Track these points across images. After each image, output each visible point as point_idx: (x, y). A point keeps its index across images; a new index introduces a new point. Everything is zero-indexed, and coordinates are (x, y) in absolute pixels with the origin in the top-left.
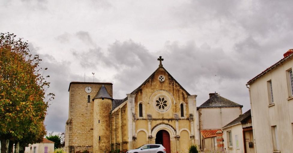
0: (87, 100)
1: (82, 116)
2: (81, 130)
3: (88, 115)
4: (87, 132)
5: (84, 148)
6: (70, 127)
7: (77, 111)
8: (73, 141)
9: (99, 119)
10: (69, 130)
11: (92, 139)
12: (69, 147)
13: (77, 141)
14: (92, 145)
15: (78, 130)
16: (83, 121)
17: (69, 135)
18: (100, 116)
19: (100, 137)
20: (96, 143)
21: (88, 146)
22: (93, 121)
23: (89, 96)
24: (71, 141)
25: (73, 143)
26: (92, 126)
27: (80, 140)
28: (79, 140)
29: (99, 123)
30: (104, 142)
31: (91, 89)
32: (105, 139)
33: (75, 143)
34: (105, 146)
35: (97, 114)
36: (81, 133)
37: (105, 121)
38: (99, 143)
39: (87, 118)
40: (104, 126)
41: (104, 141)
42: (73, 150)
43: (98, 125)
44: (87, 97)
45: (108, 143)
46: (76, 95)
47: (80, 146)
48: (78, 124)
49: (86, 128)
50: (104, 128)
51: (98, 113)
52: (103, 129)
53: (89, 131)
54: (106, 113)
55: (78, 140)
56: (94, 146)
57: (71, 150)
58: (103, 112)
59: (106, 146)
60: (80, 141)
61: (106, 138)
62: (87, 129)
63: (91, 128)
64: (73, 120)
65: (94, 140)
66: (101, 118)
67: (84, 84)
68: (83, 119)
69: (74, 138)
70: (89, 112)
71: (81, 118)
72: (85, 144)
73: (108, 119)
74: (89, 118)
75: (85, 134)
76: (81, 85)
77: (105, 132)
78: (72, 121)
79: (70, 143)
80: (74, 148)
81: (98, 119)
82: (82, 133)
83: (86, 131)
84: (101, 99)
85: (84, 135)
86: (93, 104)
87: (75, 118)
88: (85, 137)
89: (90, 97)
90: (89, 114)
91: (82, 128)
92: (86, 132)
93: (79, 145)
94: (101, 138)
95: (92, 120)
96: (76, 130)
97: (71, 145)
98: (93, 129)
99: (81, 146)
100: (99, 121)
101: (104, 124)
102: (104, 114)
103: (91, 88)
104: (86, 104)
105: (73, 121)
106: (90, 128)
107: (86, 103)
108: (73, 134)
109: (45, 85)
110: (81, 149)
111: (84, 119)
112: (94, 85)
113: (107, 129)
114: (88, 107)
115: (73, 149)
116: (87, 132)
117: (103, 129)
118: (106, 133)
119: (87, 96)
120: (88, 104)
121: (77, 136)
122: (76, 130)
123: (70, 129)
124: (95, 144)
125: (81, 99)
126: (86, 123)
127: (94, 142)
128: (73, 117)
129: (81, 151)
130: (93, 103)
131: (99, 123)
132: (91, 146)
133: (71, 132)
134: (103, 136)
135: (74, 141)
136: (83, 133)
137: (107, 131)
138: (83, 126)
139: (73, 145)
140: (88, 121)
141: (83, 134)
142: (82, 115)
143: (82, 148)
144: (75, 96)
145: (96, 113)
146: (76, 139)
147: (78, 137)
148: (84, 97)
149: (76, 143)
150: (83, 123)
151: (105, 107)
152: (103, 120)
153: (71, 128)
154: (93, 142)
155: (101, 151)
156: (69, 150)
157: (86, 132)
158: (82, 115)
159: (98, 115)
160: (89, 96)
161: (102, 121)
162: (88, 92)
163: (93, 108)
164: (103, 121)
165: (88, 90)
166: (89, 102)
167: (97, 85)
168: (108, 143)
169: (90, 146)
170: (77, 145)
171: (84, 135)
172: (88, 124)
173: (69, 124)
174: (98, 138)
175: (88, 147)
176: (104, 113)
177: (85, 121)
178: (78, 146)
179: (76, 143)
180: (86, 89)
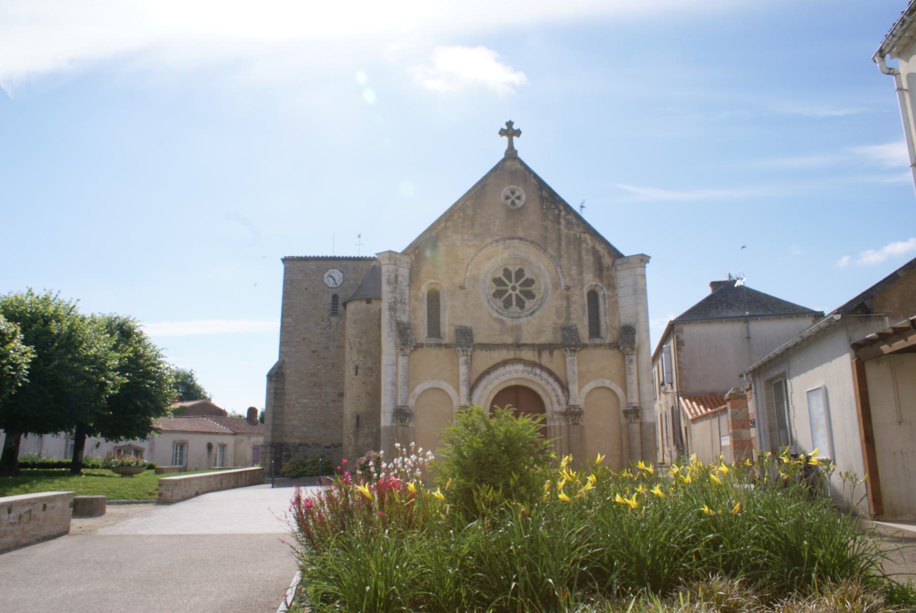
6: (108, 573)
18: (359, 352)
19: (358, 417)
21: (329, 444)
44: (330, 300)
81: (353, 362)
120: (333, 319)
131: (356, 374)
169: (336, 444)
174: (354, 421)
175: (329, 447)
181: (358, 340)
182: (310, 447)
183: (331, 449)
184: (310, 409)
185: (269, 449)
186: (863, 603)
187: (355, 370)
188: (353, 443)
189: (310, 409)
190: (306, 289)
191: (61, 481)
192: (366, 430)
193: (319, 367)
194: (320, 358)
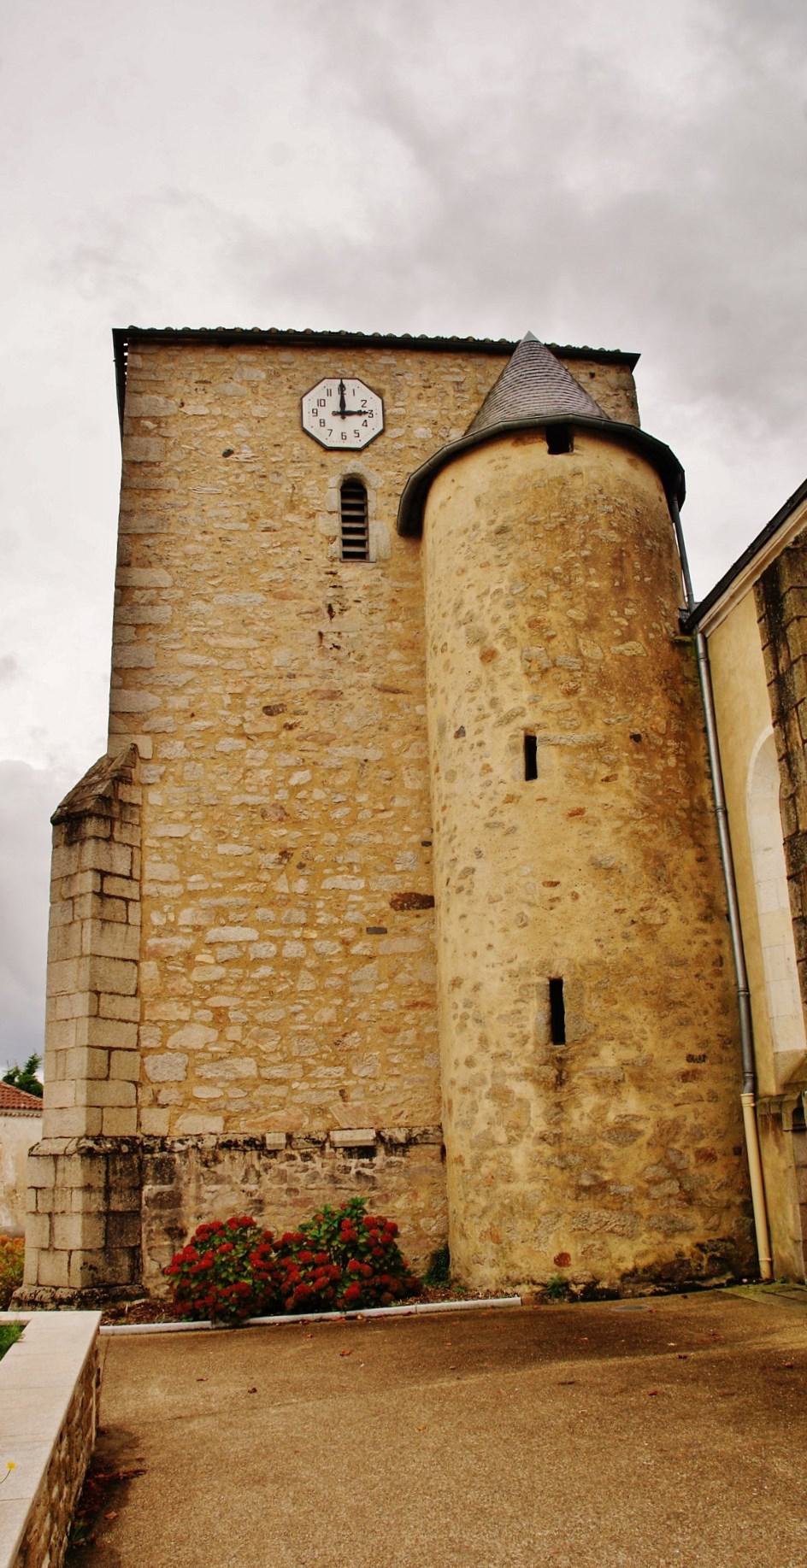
0: (331, 524)
1: (271, 724)
2: (270, 914)
3: (349, 719)
4: (345, 943)
5: (316, 1164)
6: (103, 874)
7: (199, 659)
8: (150, 1061)
9: (529, 720)
10: (87, 906)
11: (429, 1045)
12: (89, 1154)
13: (207, 1071)
14: (422, 1121)
15: (221, 915)
16: (282, 795)
17: (85, 977)
18: (540, 673)
19: (556, 986)
20: (501, 1095)
21: (366, 1137)
22: (425, 797)
23: (354, 490)
24: (124, 1065)
25: (155, 1102)
26: (407, 858)
27: (256, 1053)
28: (237, 1050)
29: (531, 772)
30: (640, 1076)
31: (374, 403)
32: (640, 1017)
33: (188, 1103)
34: (648, 1129)
35: (488, 656)
36: (267, 950)
37: (620, 742)
38: (558, 1080)
39: (342, 753)
40: (606, 828)
41: (630, 1054)
42: (159, 1201)
43: (509, 816)
44: (334, 499)
45: (685, 1077)
46: (183, 476)
47: (257, 1145)
48: (221, 836)
49: (340, 882)
50: (621, 855)
51: (511, 641)
52: (604, 870)
53: (381, 931)
54: (628, 636)
55: (217, 1059)
56: (458, 1142)
57: (117, 1205)
58: (580, 614)
59: (668, 1132)
60: (247, 1068)
61: (664, 1002)
62: (338, 901)
63: (407, 887)
64: (147, 773)
65: (458, 1045)
66: (553, 699)
67: (286, 356)
68: (290, 770)
69: (167, 1028)
70: (369, 677)
71: (257, 754)
72: (322, 1111)
73: (654, 714)
74: (373, 754)
75: (320, 972)
76: (245, 357)
77: (632, 907)
78: (130, 794)
79: (116, 1092)
80: (166, 1171)
81: (508, 719)
82: (278, 961)
83: (328, 931)
84: (540, 448)
85: (306, 982)
86: (418, 576)
87: (175, 749)
88: (327, 1014)
89: (363, 507)
90: (361, 707)
91: (282, 886)
92: (330, 947)
93: (243, 1129)
94: (582, 1011)
95: (411, 782)
96: (187, 916)
97: (121, 1126)
98: (428, 902)
99: (275, 1139)
100: (530, 745)
101: (607, 795)
102: (592, 651)
103: (379, 393)
104: (311, 577)
105: (154, 797)
106: (390, 884)
107: (321, 560)
108: (150, 968)
109: (201, 1047)
110: (270, 1187)
111: (301, 766)
112: (410, 361)
113: (657, 865)
114: (352, 621)
115: (149, 1189)
116: (345, 943)
117: (604, 870)
118: (649, 931)
119: (335, 481)
120: (351, 573)
121: (205, 991)
122: (187, 916)
123: (101, 895)
124: (487, 1106)
125: (253, 518)
126: (331, 825)
127: (456, 1074)
128: (146, 749)
129: (279, 1222)
130: (410, 566)
131: (531, 772)
132: (411, 1141)
133: (118, 942)
134: (611, 976)
135: (163, 1068)
136: (293, 950)
137: (664, 902)
138: (285, 854)
139: (156, 1123)
140: (354, 786)
141: (295, 965)
142: (269, 711)
143: (278, 1164)
144: (171, 481)
145: (478, 639)
146: (197, 1036)
147: (220, 1018)
148: (286, 489)
149: (202, 1092)
150: (285, 816)
151: (606, 554)
152: (596, 731)
153: (113, 886)
154: (436, 1079)
155: (588, 1206)
156: (97, 1202)
157: (330, 947)
158: (269, 711)
159: (510, 658)
160: (354, 490)
161: (579, 737)
162: (335, 432)
163: (419, 627)
164: (597, 748)
165: (343, 413)
166: (355, 548)
167: (446, 362)
168: (685, 1077)
169: (401, 1136)
170: (216, 1124)
171: (306, 982)
172: (356, 835)
173: (91, 827)
174: (536, 1013)
175: (367, 1152)
176: (591, 624)
177: (318, 794)
178: (229, 1145)
179: (202, 1092)
180: (309, 403)
181: (524, 613)
182: (274, 1153)
183: (380, 1159)
184: (265, 971)
185: (75, 1172)
186: (485, 1327)
187: (520, 758)
188: (539, 1125)
189: (265, 971)
190: (228, 453)
191: (536, 1044)
192: (609, 1057)
193: (299, 777)
194: (300, 739)
